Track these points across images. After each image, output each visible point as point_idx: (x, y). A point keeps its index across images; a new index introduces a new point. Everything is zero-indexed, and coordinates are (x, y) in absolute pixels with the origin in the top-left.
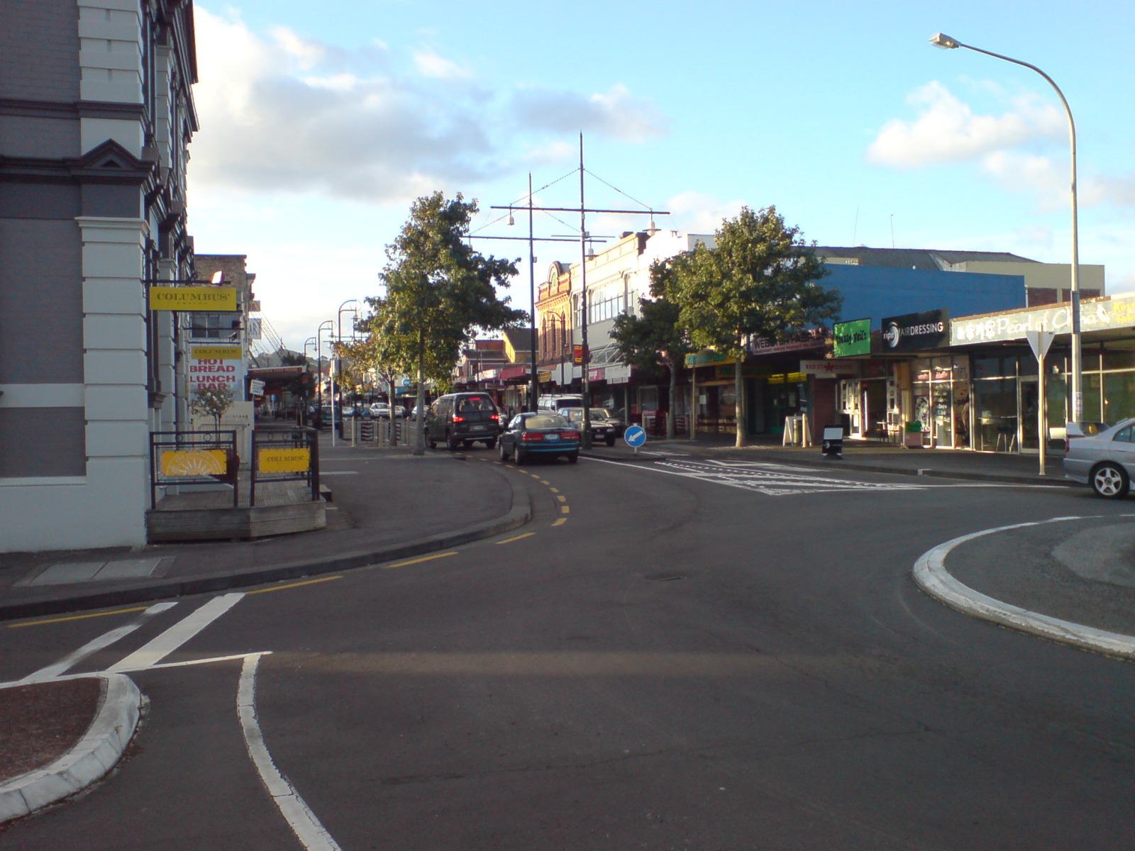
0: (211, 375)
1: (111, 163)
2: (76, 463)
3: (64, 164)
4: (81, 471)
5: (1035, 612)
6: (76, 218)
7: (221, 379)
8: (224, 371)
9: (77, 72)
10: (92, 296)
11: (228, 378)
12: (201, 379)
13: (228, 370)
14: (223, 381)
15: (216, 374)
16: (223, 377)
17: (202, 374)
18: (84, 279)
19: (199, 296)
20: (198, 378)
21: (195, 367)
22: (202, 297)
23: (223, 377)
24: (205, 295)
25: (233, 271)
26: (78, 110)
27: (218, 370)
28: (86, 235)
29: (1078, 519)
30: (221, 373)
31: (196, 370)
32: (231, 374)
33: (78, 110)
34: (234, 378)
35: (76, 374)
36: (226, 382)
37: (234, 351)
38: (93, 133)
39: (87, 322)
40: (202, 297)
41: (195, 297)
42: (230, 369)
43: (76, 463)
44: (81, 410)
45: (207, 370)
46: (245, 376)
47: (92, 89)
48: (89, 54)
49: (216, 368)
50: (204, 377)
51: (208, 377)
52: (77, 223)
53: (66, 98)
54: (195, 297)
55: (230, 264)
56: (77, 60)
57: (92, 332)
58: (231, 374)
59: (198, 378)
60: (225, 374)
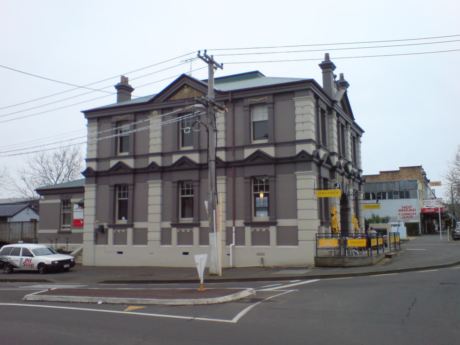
0: (407, 212)
1: (303, 157)
2: (295, 242)
3: (292, 158)
4: (297, 244)
5: (151, 283)
6: (295, 173)
7: (411, 214)
8: (411, 211)
9: (295, 132)
10: (300, 194)
11: (413, 214)
12: (403, 214)
13: (413, 211)
14: (412, 215)
15: (409, 212)
16: (412, 213)
17: (404, 212)
18: (297, 190)
19: (330, 192)
20: (402, 214)
21: (401, 210)
22: (331, 193)
23: (412, 213)
24: (332, 192)
25: (417, 172)
26: (295, 142)
27: (409, 211)
28: (298, 177)
29: (319, 281)
30: (411, 212)
31: (401, 211)
32: (414, 212)
33: (295, 142)
34: (415, 214)
35: (295, 216)
36: (413, 215)
37: (378, 206)
38: (299, 148)
39: (298, 202)
40: (331, 193)
41: (329, 193)
42: (414, 210)
43: (295, 242)
44: (297, 227)
45: (406, 211)
46: (420, 213)
47: (299, 137)
48: (298, 127)
49: (409, 210)
50: (404, 214)
51: (406, 214)
52: (295, 174)
53: (292, 140)
54: (329, 193)
55: (416, 170)
56: (295, 129)
57: (300, 204)
58: (414, 212)
59: (402, 214)
60: (412, 212)
